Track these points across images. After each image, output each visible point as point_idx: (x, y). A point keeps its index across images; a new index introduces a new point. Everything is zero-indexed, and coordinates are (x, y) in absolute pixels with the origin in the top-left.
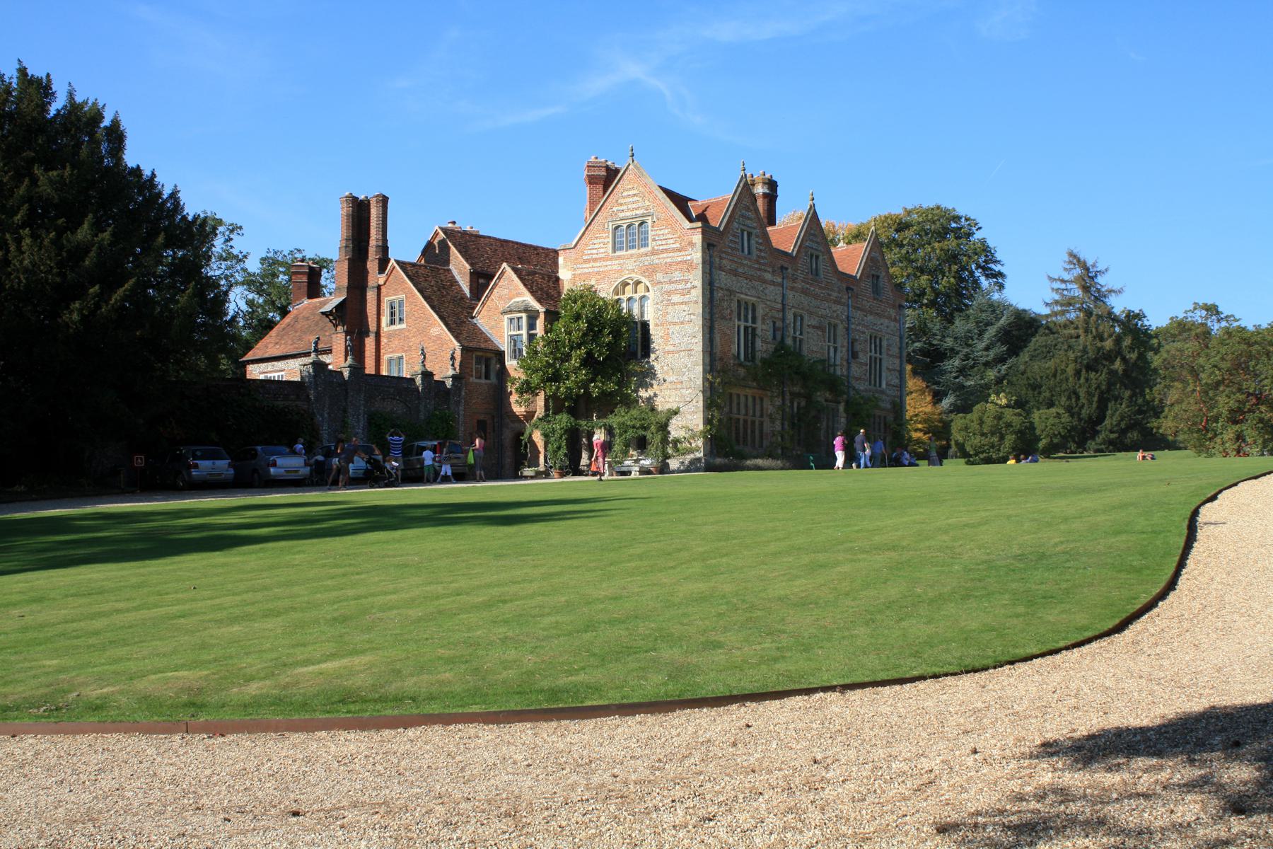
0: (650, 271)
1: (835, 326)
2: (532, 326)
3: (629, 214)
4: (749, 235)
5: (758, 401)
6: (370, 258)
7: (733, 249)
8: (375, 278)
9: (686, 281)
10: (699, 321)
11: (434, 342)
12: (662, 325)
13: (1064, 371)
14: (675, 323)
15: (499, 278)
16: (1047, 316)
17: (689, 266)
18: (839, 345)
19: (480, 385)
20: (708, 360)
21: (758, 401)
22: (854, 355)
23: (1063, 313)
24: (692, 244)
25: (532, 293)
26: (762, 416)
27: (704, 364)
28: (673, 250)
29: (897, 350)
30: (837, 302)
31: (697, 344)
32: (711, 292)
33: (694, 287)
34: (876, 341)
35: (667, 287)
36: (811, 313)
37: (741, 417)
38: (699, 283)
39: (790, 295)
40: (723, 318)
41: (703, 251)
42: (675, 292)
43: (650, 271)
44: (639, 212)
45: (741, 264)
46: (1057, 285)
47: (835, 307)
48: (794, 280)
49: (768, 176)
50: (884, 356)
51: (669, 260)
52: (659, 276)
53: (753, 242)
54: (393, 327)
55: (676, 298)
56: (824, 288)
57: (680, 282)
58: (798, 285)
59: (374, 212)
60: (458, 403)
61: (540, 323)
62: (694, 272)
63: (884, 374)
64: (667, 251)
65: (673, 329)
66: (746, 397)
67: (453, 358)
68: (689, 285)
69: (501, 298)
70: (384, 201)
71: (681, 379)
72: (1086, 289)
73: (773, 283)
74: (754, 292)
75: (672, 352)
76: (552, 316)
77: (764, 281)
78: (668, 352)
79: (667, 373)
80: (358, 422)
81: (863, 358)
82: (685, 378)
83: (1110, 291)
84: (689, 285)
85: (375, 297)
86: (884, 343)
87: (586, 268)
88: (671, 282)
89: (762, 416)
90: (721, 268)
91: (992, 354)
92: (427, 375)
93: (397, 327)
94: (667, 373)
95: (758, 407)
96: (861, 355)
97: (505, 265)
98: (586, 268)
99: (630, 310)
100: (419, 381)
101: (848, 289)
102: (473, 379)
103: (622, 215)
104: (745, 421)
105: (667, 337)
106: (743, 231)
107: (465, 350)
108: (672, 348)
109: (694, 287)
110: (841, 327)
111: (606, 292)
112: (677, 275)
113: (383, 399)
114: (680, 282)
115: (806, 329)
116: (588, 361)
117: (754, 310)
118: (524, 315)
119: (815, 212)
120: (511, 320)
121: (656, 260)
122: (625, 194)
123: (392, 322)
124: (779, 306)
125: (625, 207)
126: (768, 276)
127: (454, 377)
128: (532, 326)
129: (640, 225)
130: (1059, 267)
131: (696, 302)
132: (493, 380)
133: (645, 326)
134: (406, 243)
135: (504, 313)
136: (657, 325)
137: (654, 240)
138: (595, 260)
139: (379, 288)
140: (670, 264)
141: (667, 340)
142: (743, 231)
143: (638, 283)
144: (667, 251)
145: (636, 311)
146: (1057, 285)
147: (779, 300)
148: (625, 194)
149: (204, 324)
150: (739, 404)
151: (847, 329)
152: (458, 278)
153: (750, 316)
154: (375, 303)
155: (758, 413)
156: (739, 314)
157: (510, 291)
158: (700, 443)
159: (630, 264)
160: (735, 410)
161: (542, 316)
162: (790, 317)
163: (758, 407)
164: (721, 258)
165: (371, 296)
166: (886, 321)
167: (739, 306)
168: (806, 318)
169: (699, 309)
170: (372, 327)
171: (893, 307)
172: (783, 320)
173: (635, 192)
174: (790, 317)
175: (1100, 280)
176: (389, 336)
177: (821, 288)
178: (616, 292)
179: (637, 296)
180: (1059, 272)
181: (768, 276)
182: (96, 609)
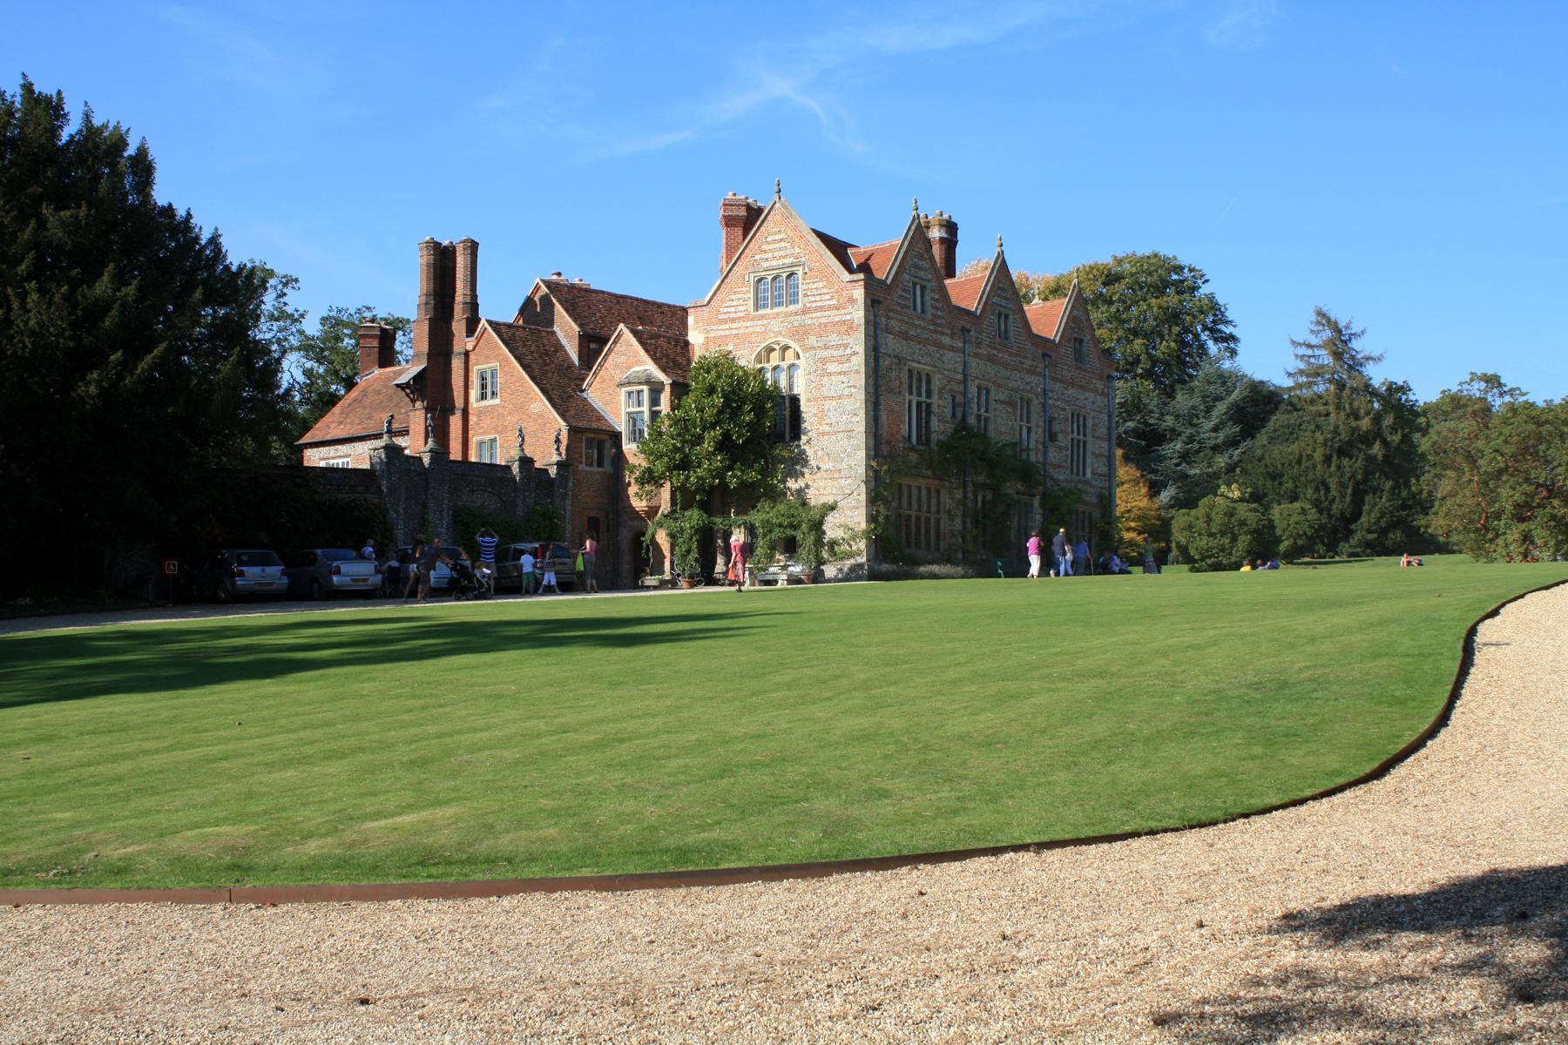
0: (801, 333)
1: (1029, 402)
2: (655, 401)
3: (774, 263)
4: (923, 289)
5: (933, 494)
6: (456, 317)
7: (903, 306)
8: (462, 342)
9: (846, 346)
10: (861, 396)
11: (535, 420)
12: (816, 400)
13: (1310, 457)
14: (832, 398)
15: (615, 342)
16: (1290, 389)
17: (849, 327)
18: (1033, 424)
19: (592, 473)
20: (872, 443)
21: (933, 494)
22: (1052, 437)
23: (1309, 385)
24: (852, 301)
25: (656, 360)
26: (938, 512)
27: (867, 448)
28: (829, 308)
29: (1105, 431)
30: (1031, 372)
31: (859, 424)
32: (876, 359)
33: (855, 353)
34: (1079, 419)
35: (822, 353)
36: (999, 385)
37: (913, 514)
38: (861, 349)
39: (973, 363)
40: (891, 391)
41: (866, 309)
42: (832, 359)
43: (801, 333)
44: (788, 261)
45: (913, 325)
46: (1302, 351)
47: (1028, 378)
48: (979, 345)
49: (945, 216)
50: (1089, 438)
51: (824, 320)
52: (812, 340)
53: (927, 298)
54: (484, 403)
55: (832, 367)
56: (1015, 355)
57: (837, 347)
58: (983, 351)
59: (461, 261)
60: (564, 496)
61: (665, 398)
62: (854, 335)
63: (1088, 461)
64: (821, 309)
65: (829, 405)
66: (919, 488)
67: (558, 441)
68: (849, 351)
69: (617, 366)
70: (473, 247)
71: (838, 466)
72: (1337, 356)
73: (952, 348)
74: (928, 360)
75: (828, 433)
76: (680, 389)
77: (941, 346)
78: (823, 434)
79: (821, 459)
80: (441, 519)
81: (1064, 441)
82: (844, 465)
83: (1368, 358)
84: (849, 351)
85: (462, 365)
86: (1089, 423)
87: (721, 330)
88: (826, 347)
89: (938, 512)
90: (888, 330)
91: (1222, 435)
92: (526, 462)
93: (489, 402)
94: (821, 459)
95: (933, 501)
96: (1060, 437)
97: (621, 326)
98: (721, 330)
99: (776, 382)
100: (515, 469)
101: (1044, 355)
102: (582, 467)
103: (766, 264)
104: (918, 519)
105: (821, 415)
106: (915, 284)
107: (573, 430)
108: (827, 429)
109: (855, 353)
110: (1035, 402)
111: (746, 359)
112: (834, 339)
113: (472, 491)
114: (837, 347)
115: (992, 404)
116: (724, 444)
117: (929, 382)
118: (645, 388)
119: (1004, 261)
120: (630, 393)
121: (807, 319)
122: (770, 238)
123: (483, 397)
124: (960, 377)
125: (769, 255)
126: (946, 340)
127: (559, 464)
128: (655, 401)
129: (789, 277)
130: (1304, 328)
131: (857, 372)
132: (608, 467)
133: (795, 401)
134: (500, 299)
135: (621, 385)
136: (809, 400)
137: (806, 295)
138: (733, 320)
139: (467, 354)
140: (826, 325)
141: (821, 419)
142: (915, 284)
143: (786, 348)
144: (821, 309)
145: (783, 383)
146: (1302, 351)
147: (960, 369)
148: (770, 238)
149: (252, 399)
150: (910, 497)
151: (1044, 405)
152: (564, 342)
153: (924, 389)
154: (462, 372)
155: (933, 509)
156: (910, 387)
157: (628, 358)
158: (862, 545)
159: (776, 325)
160: (905, 505)
161: (668, 389)
162: (973, 390)
163: (933, 501)
164: (888, 318)
165: (457, 364)
166: (1091, 396)
167: (910, 377)
168: (993, 391)
169: (861, 380)
170: (459, 402)
171: (1100, 377)
172: (965, 393)
173: (782, 236)
174: (973, 390)
175: (1355, 344)
176: (480, 413)
177: (1011, 354)
178: (759, 359)
179: (784, 365)
180: (1304, 335)
181: (946, 340)
182: (118, 749)
